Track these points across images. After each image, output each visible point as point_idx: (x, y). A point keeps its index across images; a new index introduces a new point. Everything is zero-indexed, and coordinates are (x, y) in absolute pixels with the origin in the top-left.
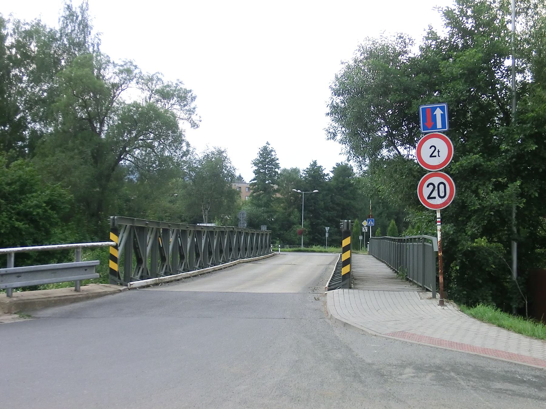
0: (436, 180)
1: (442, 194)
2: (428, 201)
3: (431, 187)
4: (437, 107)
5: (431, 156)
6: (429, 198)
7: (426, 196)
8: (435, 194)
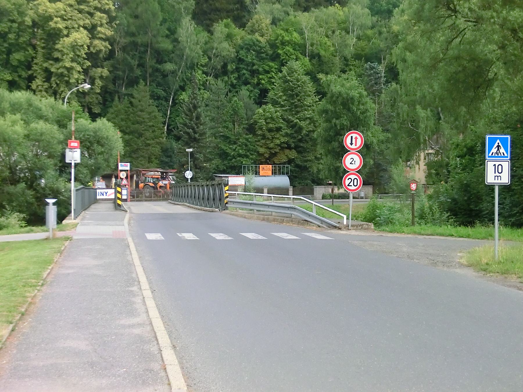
0: (353, 177)
1: (355, 184)
2: (348, 187)
3: (350, 180)
4: (497, 138)
5: (351, 163)
6: (348, 185)
7: (347, 184)
8: (352, 184)
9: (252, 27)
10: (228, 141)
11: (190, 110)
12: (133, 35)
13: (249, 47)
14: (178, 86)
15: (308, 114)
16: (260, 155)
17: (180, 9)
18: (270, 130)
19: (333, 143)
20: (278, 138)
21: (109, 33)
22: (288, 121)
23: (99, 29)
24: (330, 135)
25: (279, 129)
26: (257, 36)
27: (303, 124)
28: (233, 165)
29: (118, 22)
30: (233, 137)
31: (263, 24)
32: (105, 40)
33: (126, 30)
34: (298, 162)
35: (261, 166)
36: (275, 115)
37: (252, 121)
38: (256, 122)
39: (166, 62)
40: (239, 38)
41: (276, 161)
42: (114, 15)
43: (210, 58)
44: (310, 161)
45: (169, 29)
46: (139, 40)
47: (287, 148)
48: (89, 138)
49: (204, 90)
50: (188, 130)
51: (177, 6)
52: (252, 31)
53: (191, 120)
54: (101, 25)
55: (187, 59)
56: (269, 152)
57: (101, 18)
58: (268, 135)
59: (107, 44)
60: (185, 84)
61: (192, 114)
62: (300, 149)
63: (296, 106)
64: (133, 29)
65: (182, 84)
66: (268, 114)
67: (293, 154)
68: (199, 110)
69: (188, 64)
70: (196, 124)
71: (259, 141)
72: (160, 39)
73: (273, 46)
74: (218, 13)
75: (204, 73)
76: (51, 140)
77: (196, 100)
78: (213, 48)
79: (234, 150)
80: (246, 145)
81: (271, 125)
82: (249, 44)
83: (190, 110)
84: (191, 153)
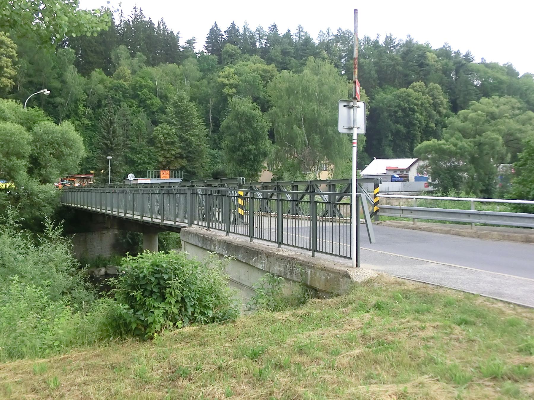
9: (118, 75)
10: (134, 151)
11: (107, 125)
12: (30, 76)
13: (117, 88)
14: (65, 115)
15: (197, 132)
16: (159, 162)
17: (65, 59)
18: (167, 143)
19: (238, 152)
20: (173, 150)
21: (13, 73)
22: (181, 137)
23: (5, 69)
24: (235, 147)
25: (173, 143)
26: (122, 81)
27: (194, 139)
28: (139, 170)
29: (19, 66)
30: (138, 148)
31: (126, 73)
32: (10, 79)
33: (26, 72)
34: (188, 168)
35: (161, 171)
36: (170, 132)
37: (152, 136)
38: (155, 137)
39: (56, 97)
40: (108, 82)
41: (171, 168)
42: (17, 60)
43: (88, 95)
44: (197, 167)
45: (58, 74)
46: (35, 80)
47: (179, 158)
48: (56, 140)
49: (84, 118)
50: (106, 142)
51: (62, 58)
52: (118, 78)
53: (108, 133)
54: (7, 67)
55: (72, 95)
56: (166, 161)
57: (7, 61)
58: (166, 147)
59: (11, 81)
60: (71, 114)
61: (109, 129)
62: (189, 158)
63: (186, 126)
64: (31, 72)
65: (68, 113)
66: (165, 131)
67: (184, 162)
68: (115, 125)
69: (73, 99)
70: (113, 137)
71: (158, 152)
72: (52, 80)
73: (134, 88)
74: (91, 65)
75: (84, 106)
76: (21, 141)
77: (112, 117)
78: (90, 89)
79: (140, 159)
80: (149, 155)
81: (168, 140)
82: (117, 86)
83: (107, 125)
84: (110, 159)
